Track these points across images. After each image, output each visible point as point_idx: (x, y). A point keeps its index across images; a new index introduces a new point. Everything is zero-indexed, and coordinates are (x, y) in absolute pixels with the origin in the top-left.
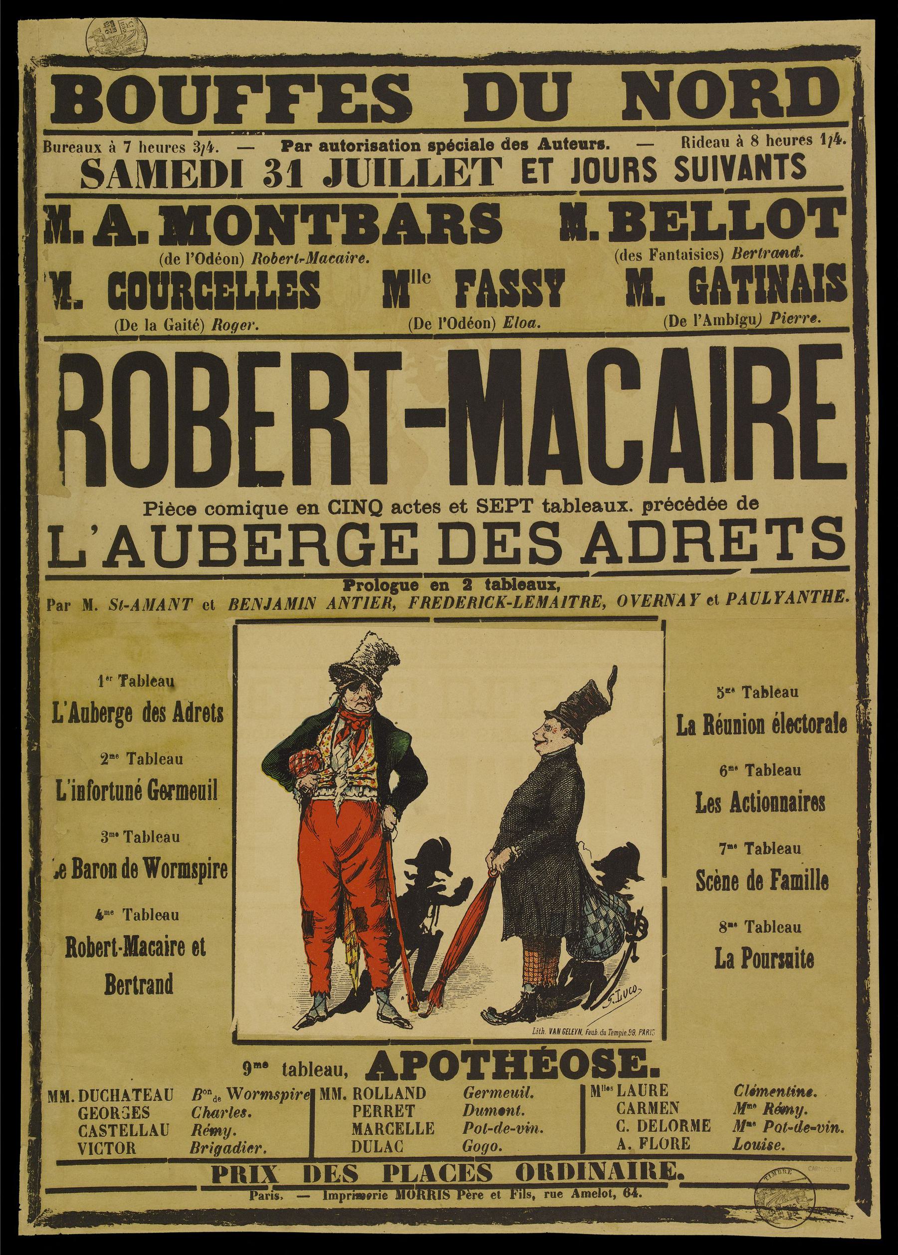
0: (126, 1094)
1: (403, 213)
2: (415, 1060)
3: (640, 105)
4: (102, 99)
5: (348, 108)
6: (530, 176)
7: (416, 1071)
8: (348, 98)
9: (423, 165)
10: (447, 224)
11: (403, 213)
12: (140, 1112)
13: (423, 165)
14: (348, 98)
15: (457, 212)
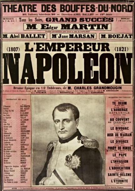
0: (126, 35)
1: (76, 35)
2: (61, 45)
3: (104, 28)
4: (112, 36)
5: (40, 37)
6: (35, 10)
7: (61, 49)
8: (70, 47)
9: (82, 11)
10: (78, 47)
11: (76, 35)
12: (89, 88)
13: (82, 11)
14: (70, 47)
15: (81, 35)
